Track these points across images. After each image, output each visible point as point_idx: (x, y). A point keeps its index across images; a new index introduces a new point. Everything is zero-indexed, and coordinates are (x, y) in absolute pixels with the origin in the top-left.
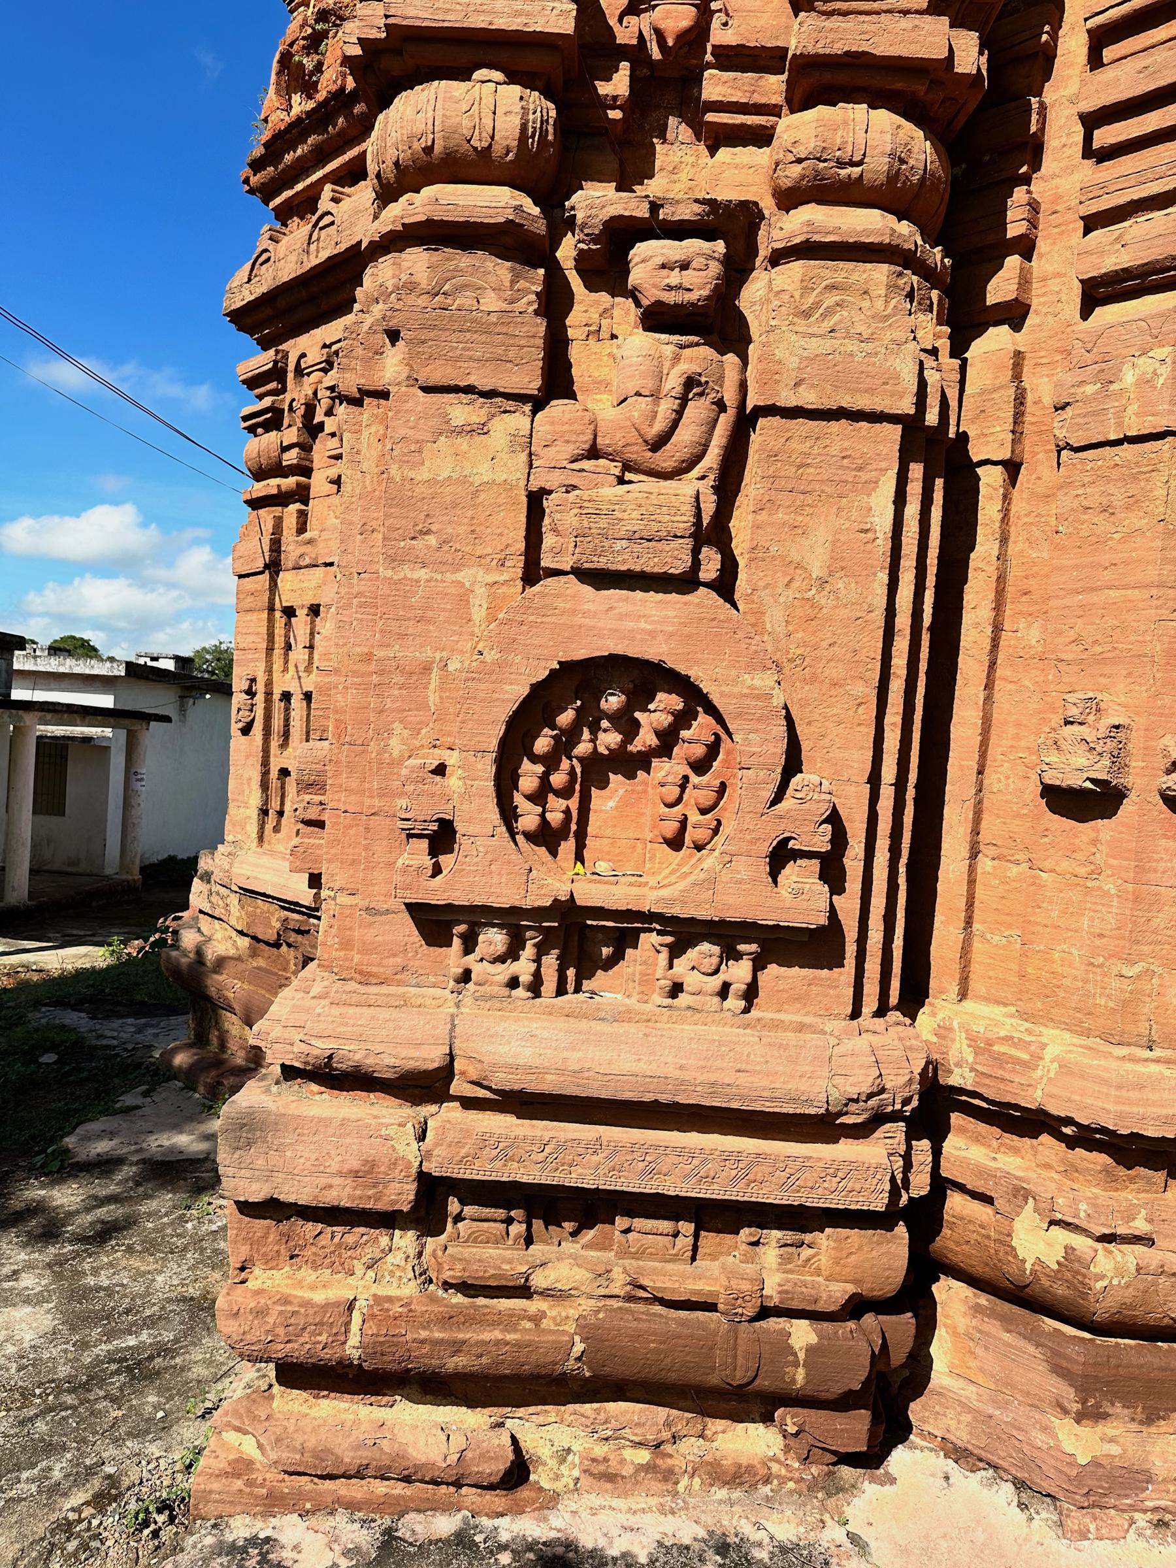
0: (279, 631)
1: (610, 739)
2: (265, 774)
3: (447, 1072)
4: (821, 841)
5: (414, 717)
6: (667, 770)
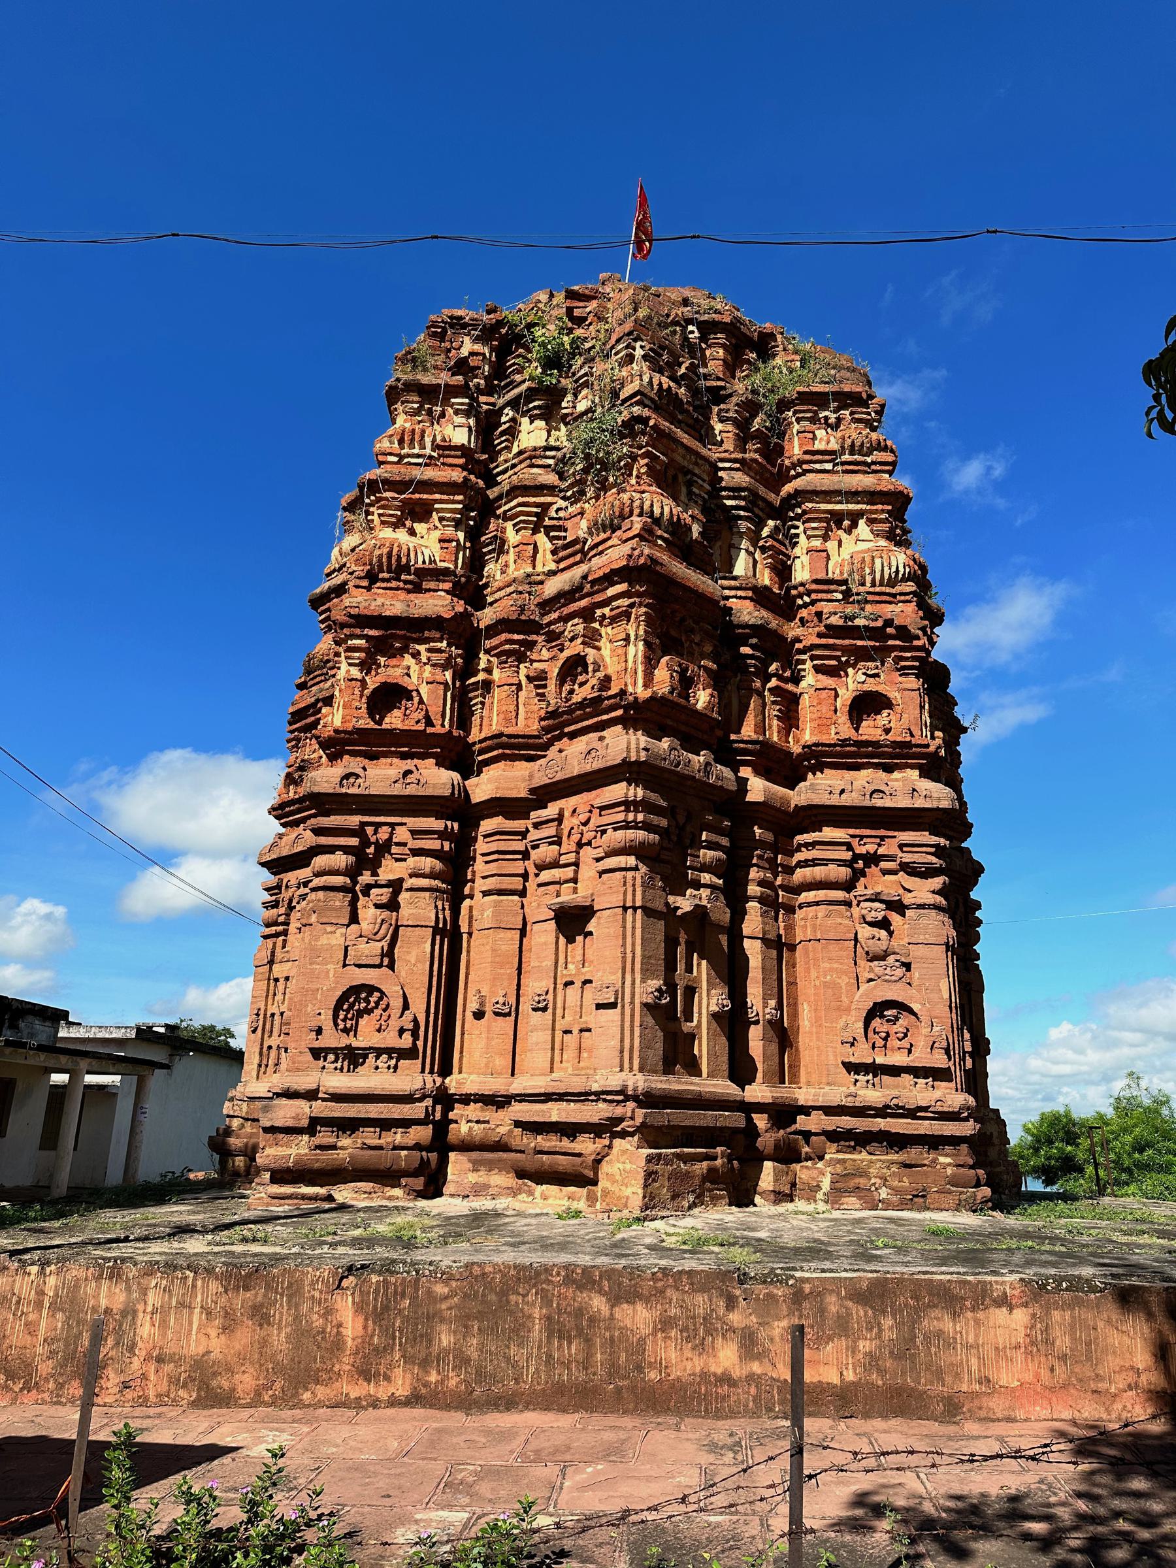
0: (272, 988)
1: (363, 1005)
2: (262, 1049)
3: (317, 1090)
4: (411, 1026)
6: (377, 1012)
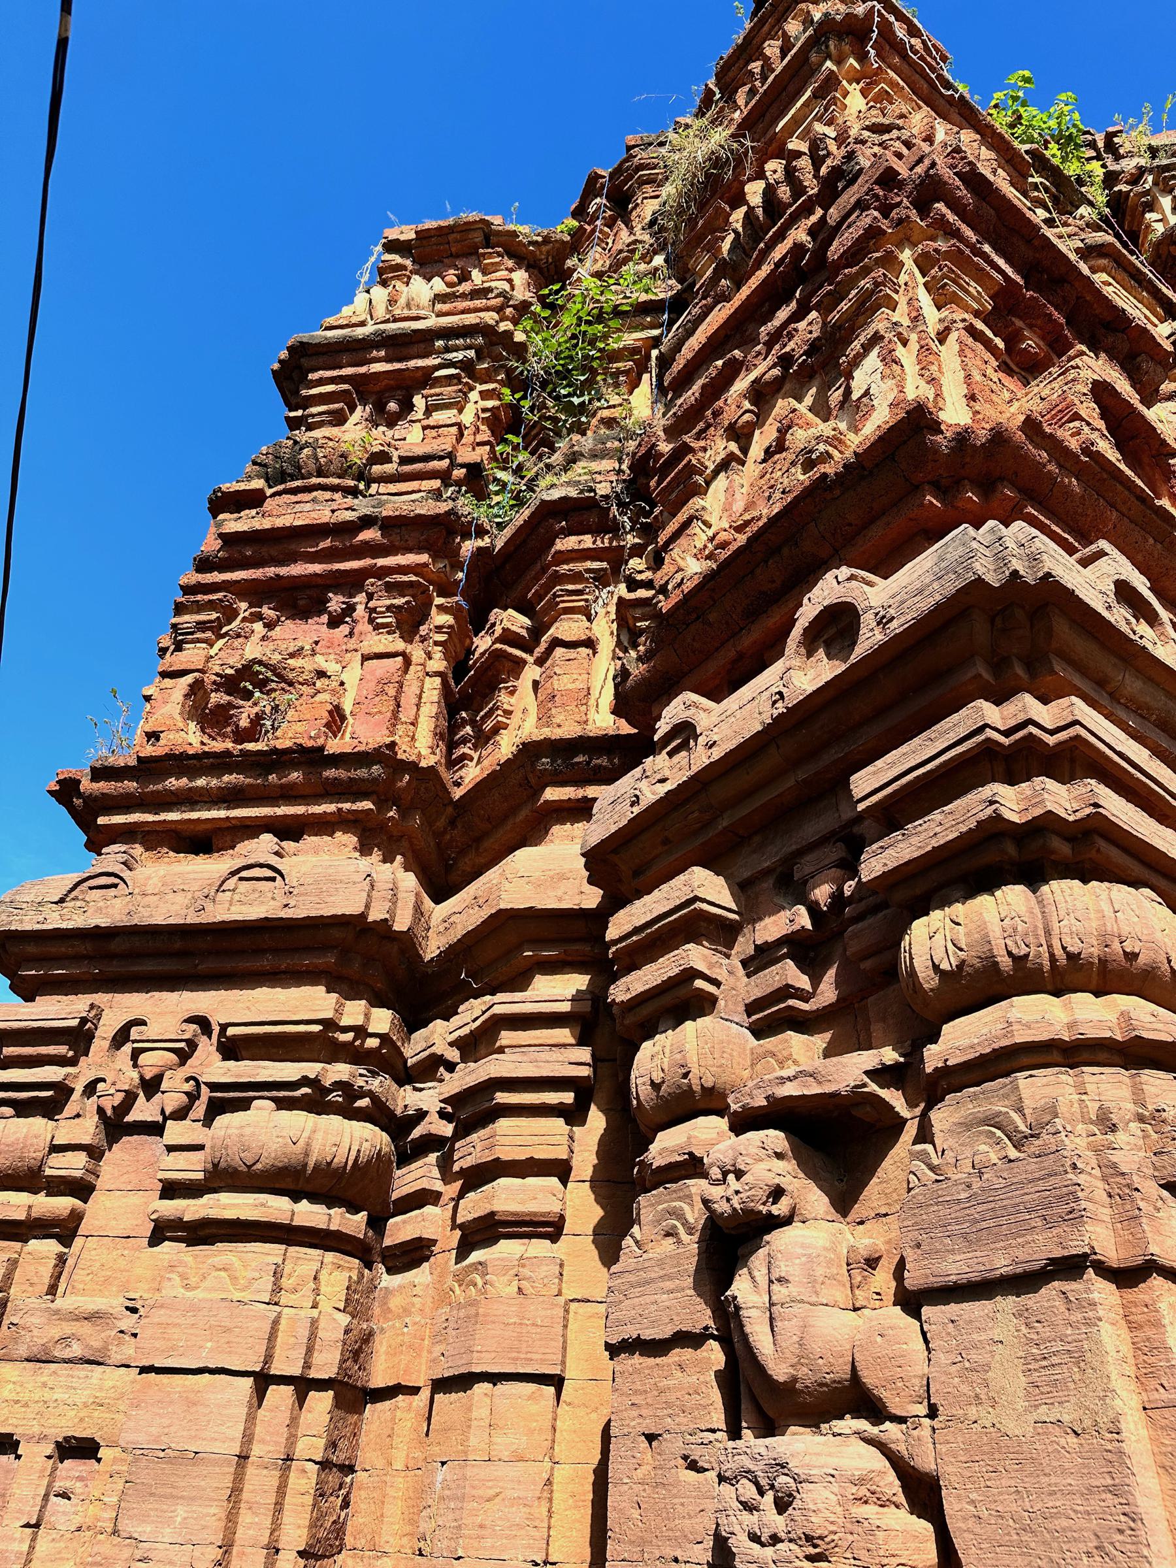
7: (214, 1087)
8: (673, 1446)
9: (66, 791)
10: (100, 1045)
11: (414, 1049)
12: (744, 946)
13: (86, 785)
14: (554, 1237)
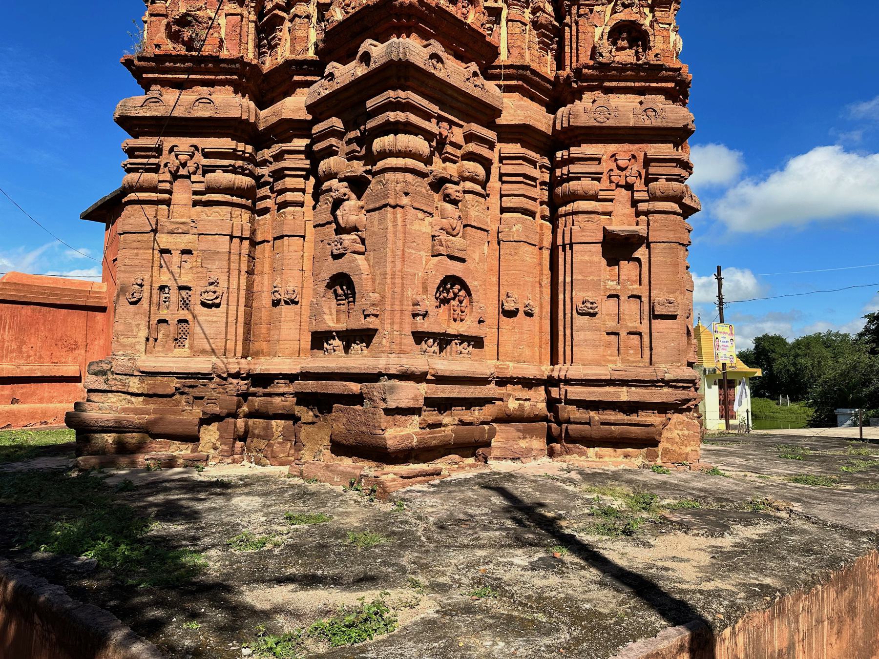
5: (413, 286)
7: (203, 166)
8: (326, 242)
9: (128, 63)
10: (165, 152)
11: (259, 157)
12: (346, 138)
13: (136, 62)
14: (302, 207)
